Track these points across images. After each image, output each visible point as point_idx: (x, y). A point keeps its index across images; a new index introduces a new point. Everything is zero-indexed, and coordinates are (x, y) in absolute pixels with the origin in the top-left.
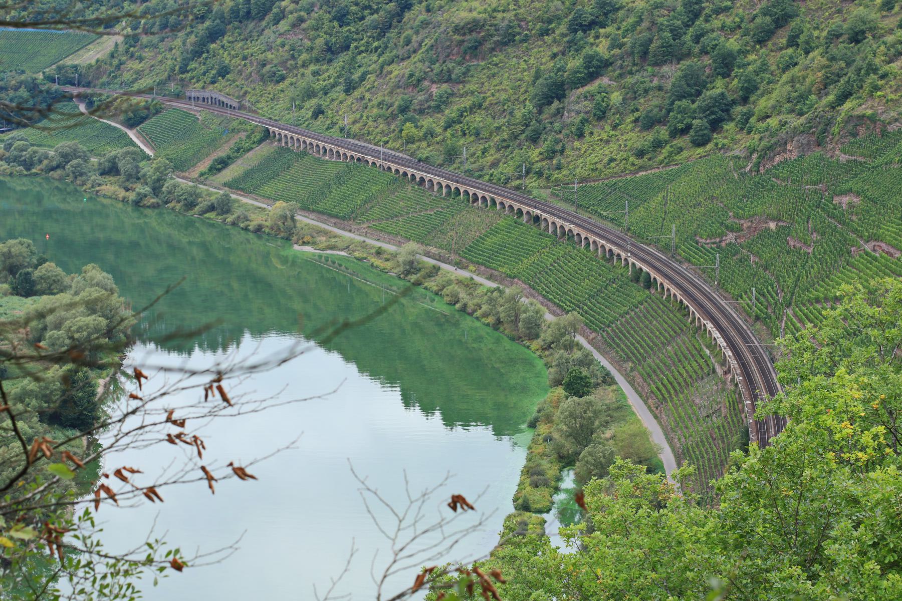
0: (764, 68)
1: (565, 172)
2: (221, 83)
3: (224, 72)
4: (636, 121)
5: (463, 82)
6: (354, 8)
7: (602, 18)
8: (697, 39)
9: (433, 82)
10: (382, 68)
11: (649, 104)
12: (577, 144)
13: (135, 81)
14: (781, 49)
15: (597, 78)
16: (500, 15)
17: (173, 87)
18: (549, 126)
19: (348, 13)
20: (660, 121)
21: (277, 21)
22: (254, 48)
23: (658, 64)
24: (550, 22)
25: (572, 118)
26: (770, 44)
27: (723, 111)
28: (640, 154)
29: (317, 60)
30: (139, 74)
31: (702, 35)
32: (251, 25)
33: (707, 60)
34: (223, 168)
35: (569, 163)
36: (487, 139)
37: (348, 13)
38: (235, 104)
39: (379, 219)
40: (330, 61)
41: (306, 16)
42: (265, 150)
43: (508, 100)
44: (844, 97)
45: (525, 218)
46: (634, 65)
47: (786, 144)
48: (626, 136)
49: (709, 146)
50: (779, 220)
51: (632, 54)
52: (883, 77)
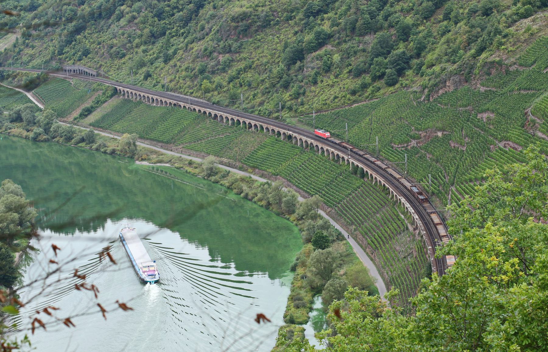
2: (85, 60)
3: (86, 53)
4: (350, 72)
5: (239, 52)
6: (167, 9)
7: (325, 8)
8: (386, 18)
9: (220, 53)
11: (358, 61)
12: (313, 88)
13: (30, 61)
14: (440, 22)
15: (323, 46)
16: (260, 9)
19: (164, 12)
21: (119, 19)
22: (105, 37)
23: (362, 35)
24: (292, 11)
25: (309, 72)
26: (432, 19)
27: (404, 63)
28: (354, 93)
29: (145, 43)
31: (389, 15)
32: (102, 23)
33: (393, 31)
34: (89, 114)
35: (308, 101)
37: (164, 12)
38: (94, 73)
39: (190, 142)
40: (154, 43)
41: (137, 15)
42: (114, 102)
44: (481, 50)
45: (282, 137)
46: (347, 36)
47: (445, 82)
48: (344, 82)
49: (397, 86)
50: (444, 130)
52: (505, 36)
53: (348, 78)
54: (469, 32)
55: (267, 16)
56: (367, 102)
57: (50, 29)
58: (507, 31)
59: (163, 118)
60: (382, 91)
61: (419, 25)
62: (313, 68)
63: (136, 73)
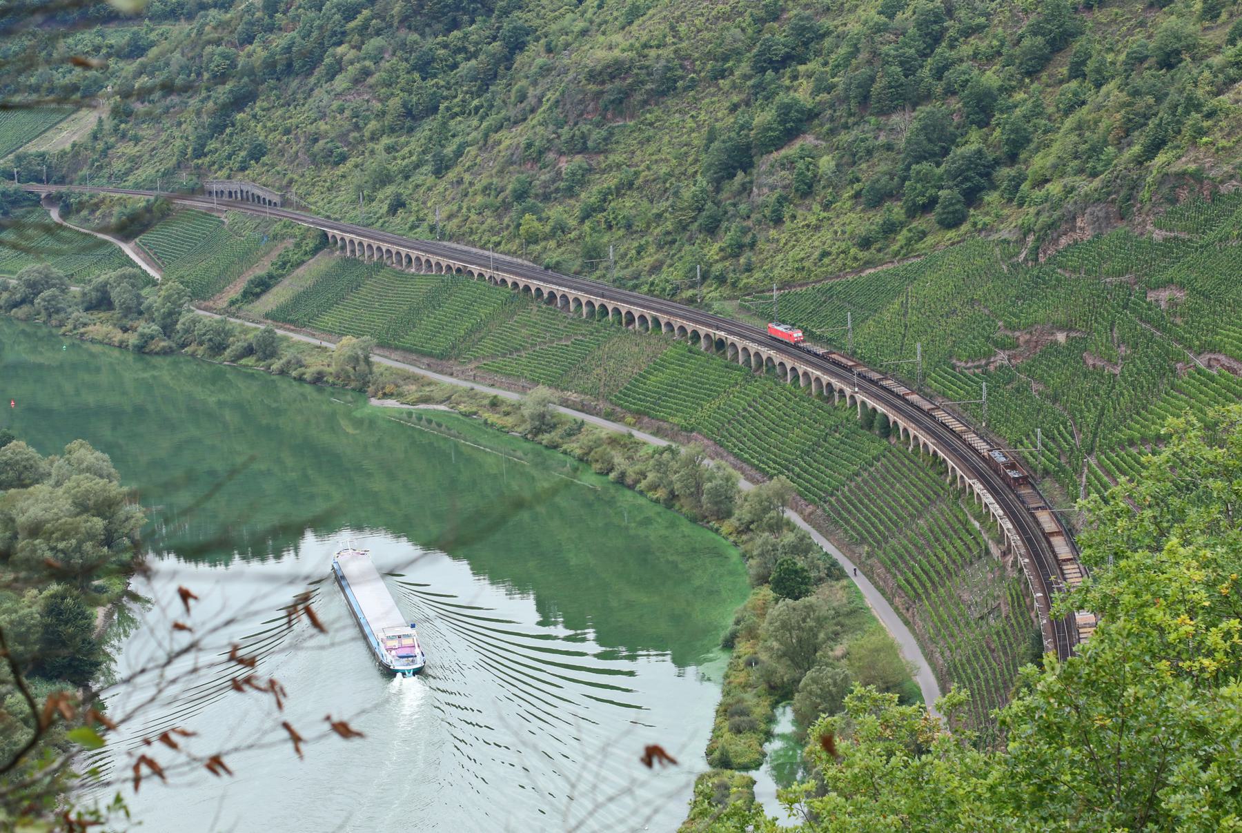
1: (758, 275)
2: (255, 169)
3: (257, 153)
4: (857, 195)
7: (800, 50)
8: (939, 74)
9: (561, 154)
11: (875, 171)
12: (773, 233)
13: (130, 170)
14: (1061, 82)
15: (797, 136)
16: (653, 53)
18: (731, 210)
19: (433, 60)
21: (331, 77)
23: (885, 112)
24: (726, 58)
25: (764, 196)
26: (1044, 76)
27: (981, 175)
28: (865, 243)
29: (392, 130)
30: (135, 162)
31: (946, 67)
32: (294, 84)
33: (955, 104)
35: (763, 262)
37: (433, 60)
38: (276, 199)
39: (493, 356)
40: (411, 130)
41: (373, 67)
42: (321, 263)
43: (670, 175)
44: (1155, 147)
45: (703, 344)
46: (851, 115)
47: (1074, 218)
49: (964, 228)
50: (1071, 329)
51: (846, 99)
52: (1210, 115)
53: (852, 209)
54: (1129, 104)
55: (670, 69)
56: (896, 264)
59: (433, 300)
60: (930, 240)
61: (1013, 88)
62: (773, 188)
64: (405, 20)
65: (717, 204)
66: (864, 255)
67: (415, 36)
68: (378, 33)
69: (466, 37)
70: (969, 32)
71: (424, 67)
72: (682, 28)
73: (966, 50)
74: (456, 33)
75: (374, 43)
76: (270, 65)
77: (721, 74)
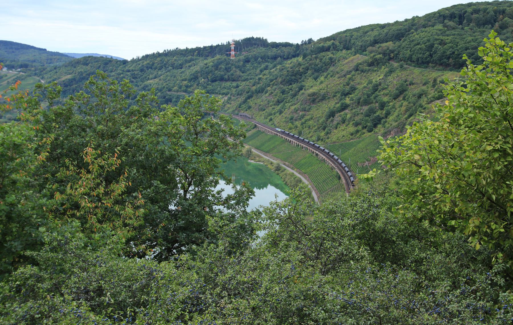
0: (394, 107)
1: (329, 140)
2: (248, 111)
3: (250, 107)
4: (353, 124)
5: (309, 111)
6: (287, 90)
7: (351, 92)
9: (301, 111)
10: (290, 107)
11: (357, 119)
12: (335, 131)
13: (228, 110)
14: (401, 101)
16: (321, 91)
17: (236, 112)
18: (328, 125)
20: (360, 124)
21: (266, 93)
22: (259, 101)
23: (362, 106)
24: (336, 93)
25: (335, 123)
26: (397, 99)
27: (378, 121)
28: (352, 134)
29: (275, 105)
30: (229, 108)
31: (377, 97)
32: (260, 94)
33: (377, 105)
35: (331, 137)
36: (312, 129)
37: (285, 91)
38: (251, 117)
39: (276, 153)
40: (278, 105)
42: (254, 131)
43: (320, 117)
45: (314, 154)
46: (356, 106)
48: (350, 129)
49: (373, 132)
51: (355, 102)
52: (424, 109)
53: (352, 127)
54: (407, 106)
57: (239, 96)
58: (426, 106)
59: (269, 140)
60: (365, 135)
61: (390, 102)
62: (337, 121)
63: (267, 118)
64: (281, 83)
65: (326, 124)
66: (351, 137)
67: (282, 86)
68: (276, 85)
69: (292, 87)
70: (384, 89)
71: (283, 92)
72: (329, 86)
73: (382, 93)
74: (291, 86)
75: (275, 87)
76: (256, 90)
77: (335, 96)
